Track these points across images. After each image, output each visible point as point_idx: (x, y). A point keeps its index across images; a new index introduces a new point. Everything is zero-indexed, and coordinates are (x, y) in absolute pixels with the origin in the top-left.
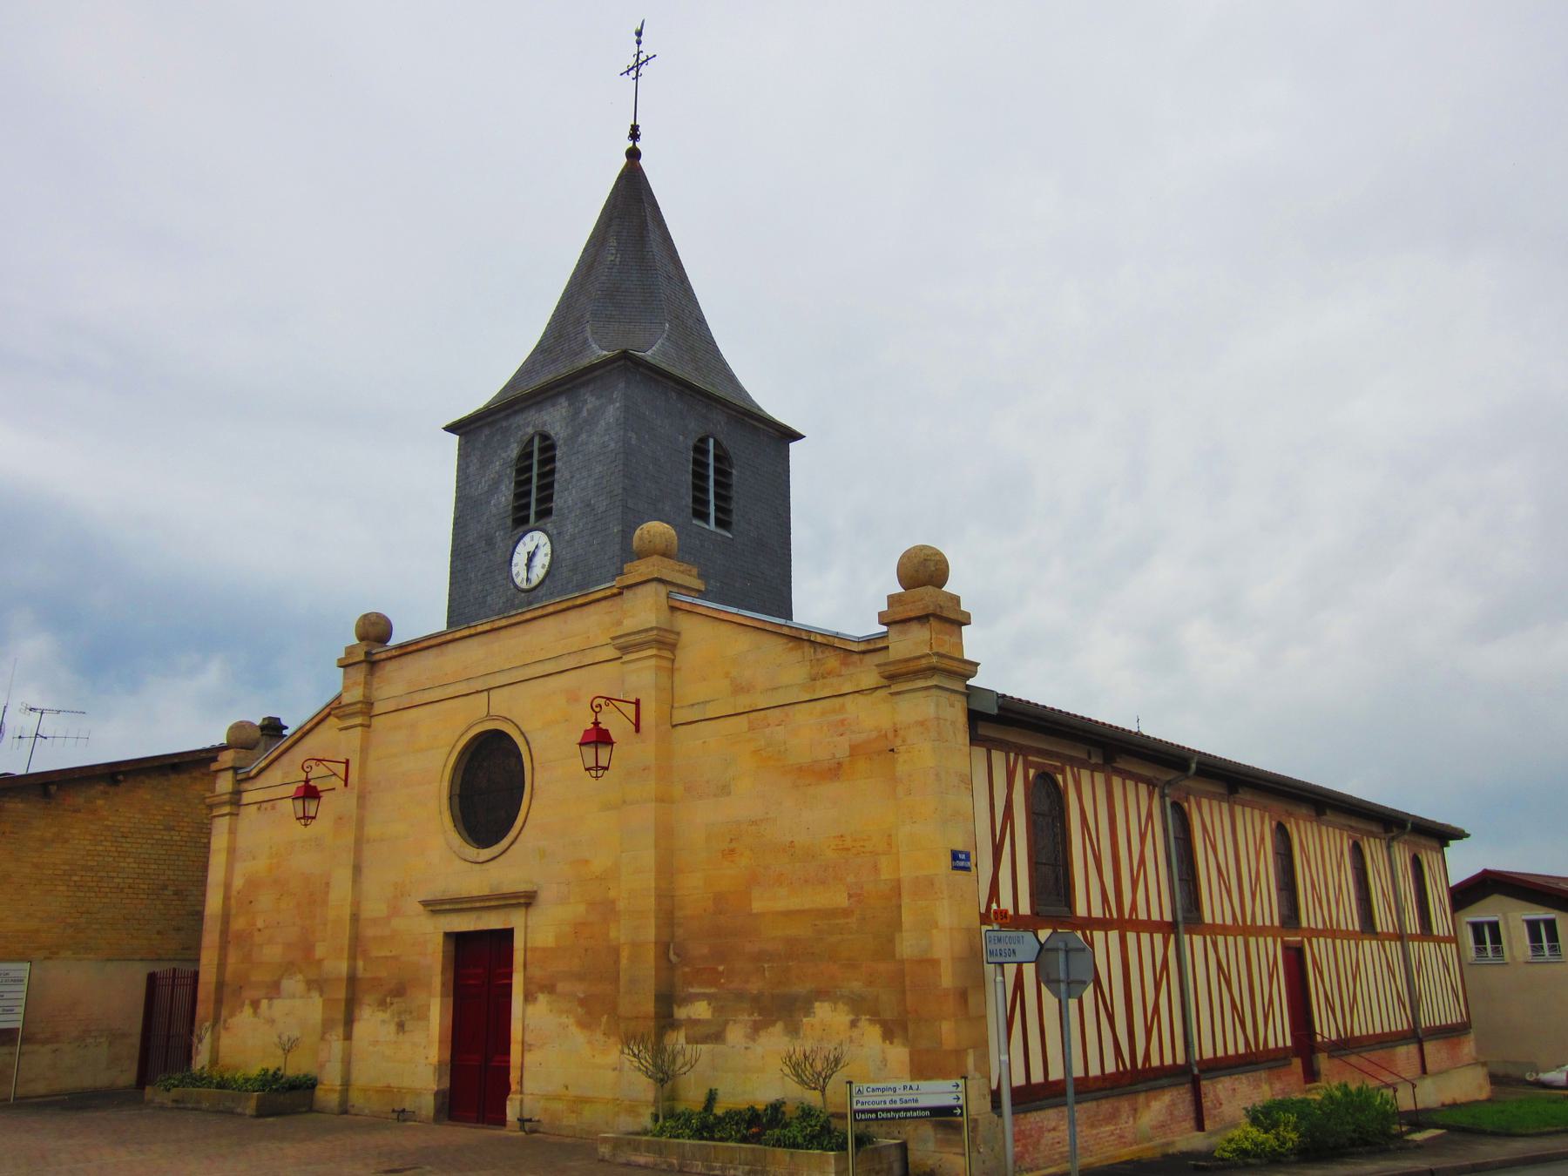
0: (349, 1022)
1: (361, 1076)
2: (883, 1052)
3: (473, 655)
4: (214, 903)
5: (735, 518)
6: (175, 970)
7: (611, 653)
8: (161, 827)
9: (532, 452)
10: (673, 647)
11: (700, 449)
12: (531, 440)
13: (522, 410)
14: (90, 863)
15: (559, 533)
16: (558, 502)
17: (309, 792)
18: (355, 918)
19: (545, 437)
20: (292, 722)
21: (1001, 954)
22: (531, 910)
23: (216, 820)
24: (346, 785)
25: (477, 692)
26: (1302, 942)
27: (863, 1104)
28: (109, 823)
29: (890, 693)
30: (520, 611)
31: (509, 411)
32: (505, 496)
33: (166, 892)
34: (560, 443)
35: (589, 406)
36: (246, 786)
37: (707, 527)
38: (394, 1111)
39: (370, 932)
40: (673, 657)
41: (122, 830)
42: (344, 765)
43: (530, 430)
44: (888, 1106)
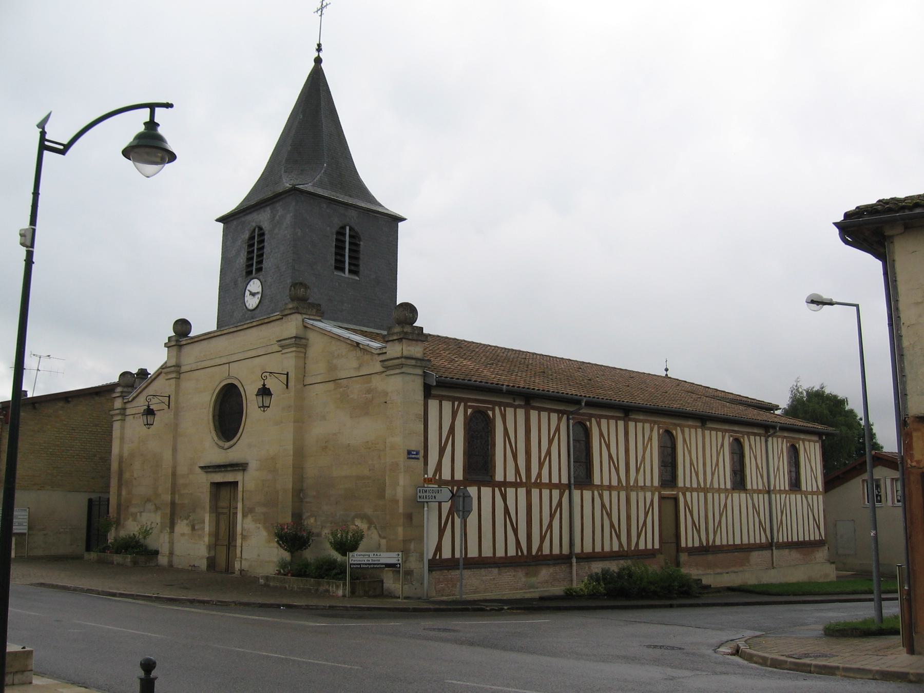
0: (172, 525)
1: (178, 550)
2: (379, 541)
3: (221, 344)
4: (114, 466)
5: (361, 268)
6: (100, 498)
7: (277, 348)
8: (92, 425)
9: (254, 236)
10: (305, 346)
11: (341, 233)
12: (254, 230)
13: (250, 213)
14: (57, 443)
15: (265, 281)
16: (265, 265)
17: (149, 412)
18: (174, 474)
19: (260, 228)
20: (152, 371)
21: (426, 498)
22: (246, 473)
23: (115, 422)
24: (169, 408)
25: (224, 364)
26: (677, 494)
27: (354, 561)
28: (66, 423)
29: (386, 375)
30: (242, 324)
31: (244, 213)
32: (242, 260)
33: (96, 458)
34: (266, 232)
35: (279, 214)
36: (128, 406)
37: (343, 275)
38: (190, 566)
39: (181, 481)
40: (305, 351)
41: (72, 426)
42: (168, 398)
43: (254, 224)
44: (366, 562)
